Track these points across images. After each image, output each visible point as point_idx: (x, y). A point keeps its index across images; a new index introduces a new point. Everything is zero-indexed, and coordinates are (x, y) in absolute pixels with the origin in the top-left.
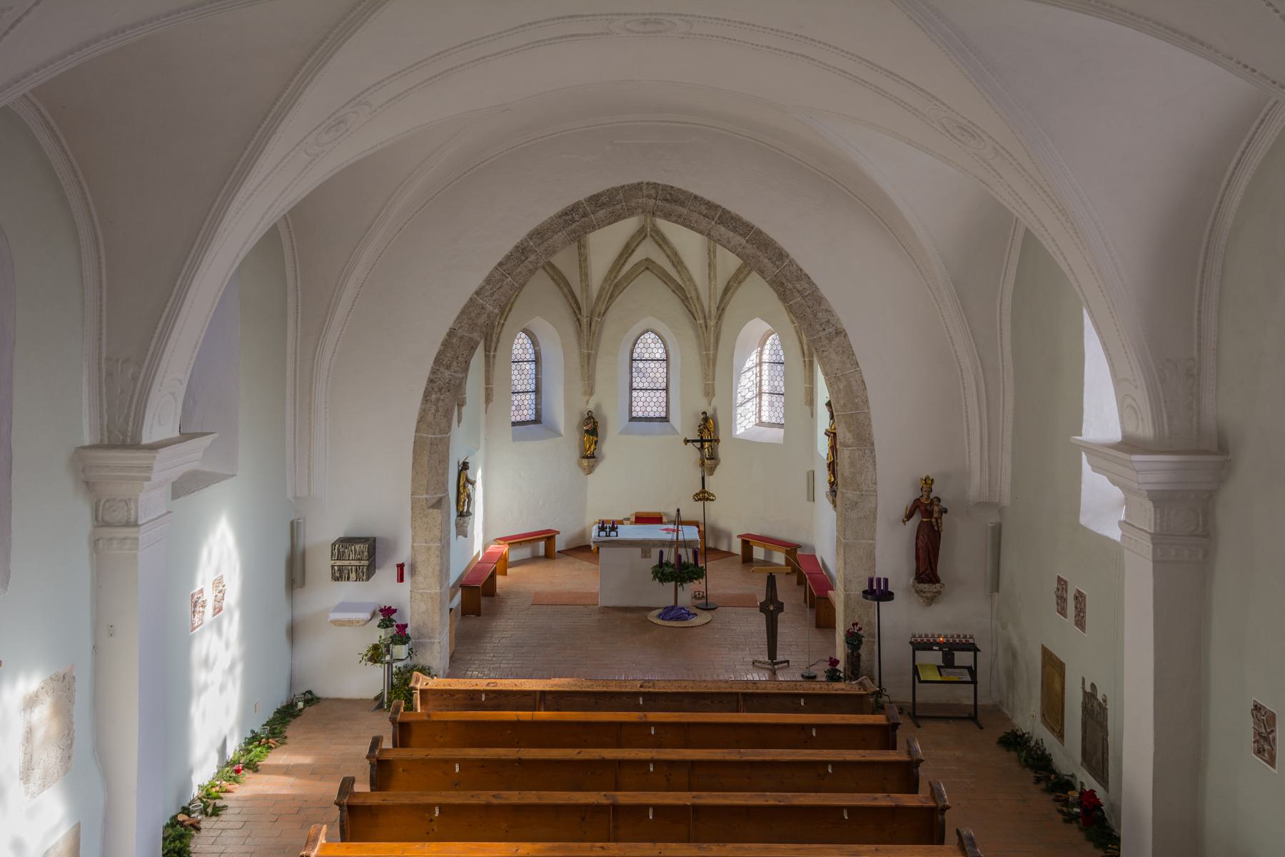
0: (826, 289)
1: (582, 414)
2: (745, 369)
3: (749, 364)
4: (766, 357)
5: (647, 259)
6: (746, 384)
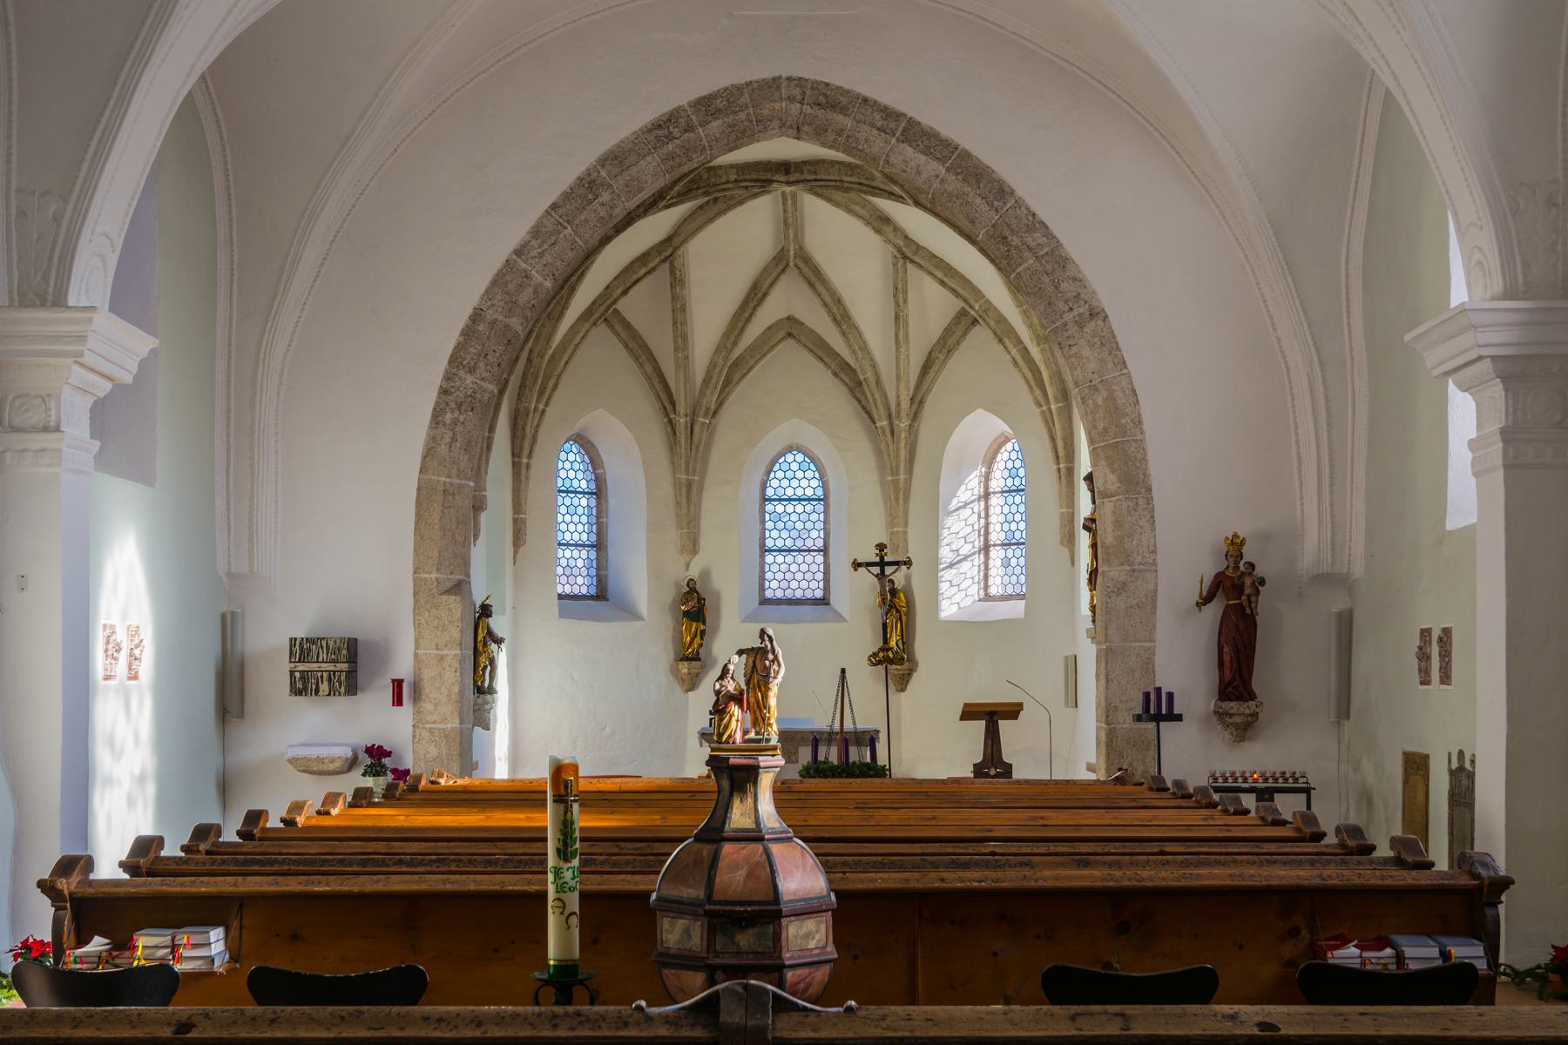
0: (1074, 243)
1: (677, 585)
2: (954, 504)
3: (964, 495)
4: (996, 484)
5: (789, 318)
6: (958, 532)
